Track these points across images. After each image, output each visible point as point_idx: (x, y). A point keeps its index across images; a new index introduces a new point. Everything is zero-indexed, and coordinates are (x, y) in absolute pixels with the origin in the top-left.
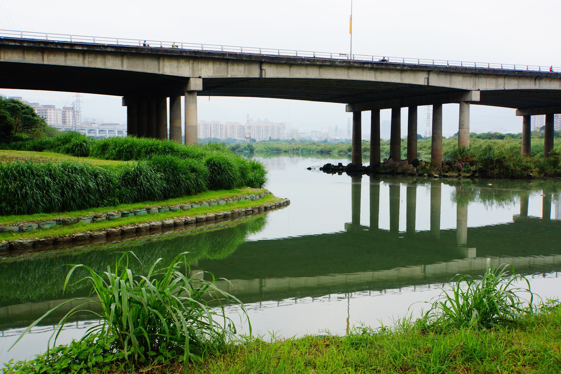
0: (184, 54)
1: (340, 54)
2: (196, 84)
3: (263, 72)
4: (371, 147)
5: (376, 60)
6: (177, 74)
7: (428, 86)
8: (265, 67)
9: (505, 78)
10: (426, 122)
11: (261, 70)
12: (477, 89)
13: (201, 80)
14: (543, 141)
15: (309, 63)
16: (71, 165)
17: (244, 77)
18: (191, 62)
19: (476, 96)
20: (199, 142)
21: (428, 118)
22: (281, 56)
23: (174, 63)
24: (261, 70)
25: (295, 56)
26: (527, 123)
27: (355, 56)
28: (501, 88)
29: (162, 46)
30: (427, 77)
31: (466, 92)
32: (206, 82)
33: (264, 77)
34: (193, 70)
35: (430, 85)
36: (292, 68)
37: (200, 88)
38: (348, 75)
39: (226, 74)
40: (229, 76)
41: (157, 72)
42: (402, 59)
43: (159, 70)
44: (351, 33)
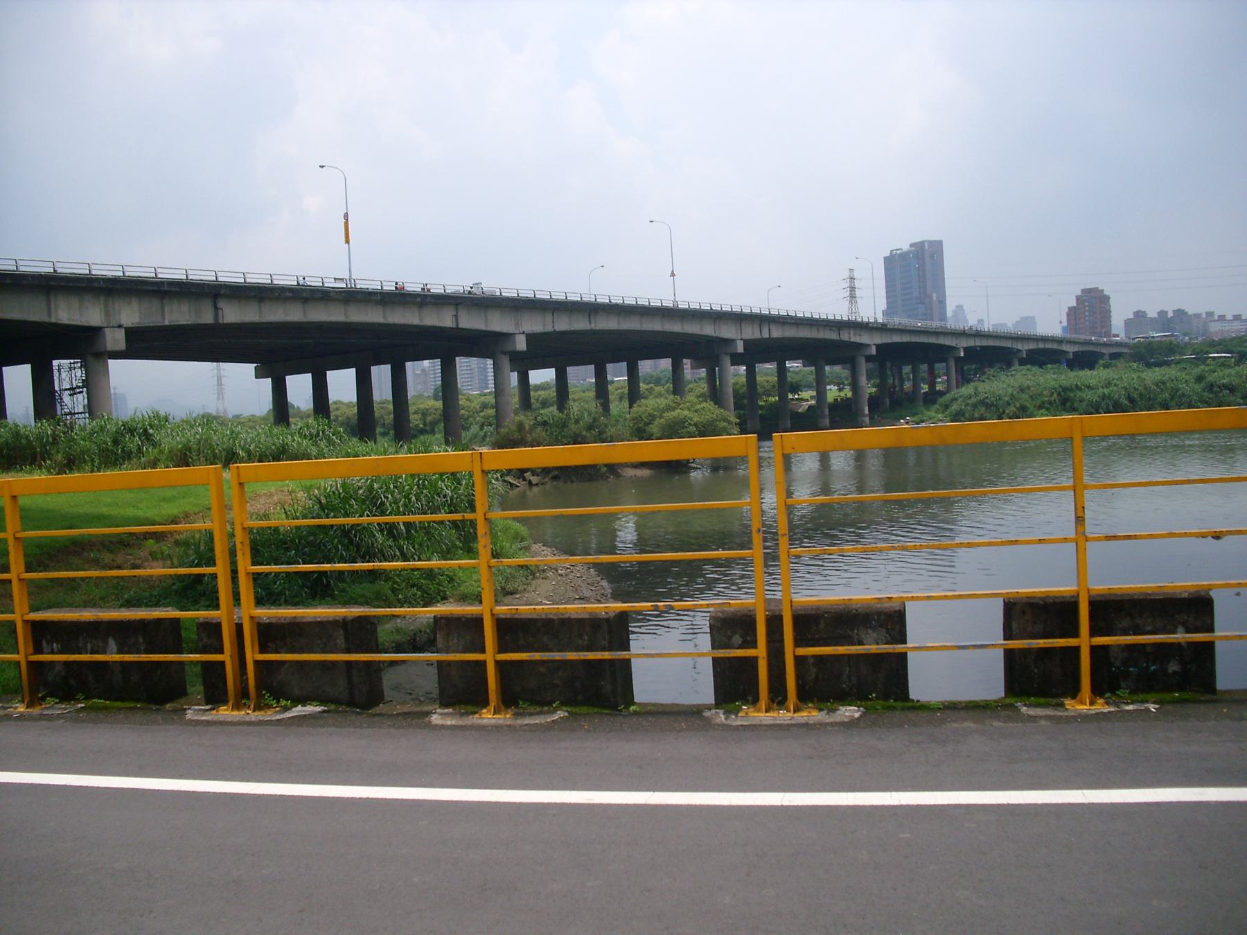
0: (96, 285)
1: (335, 279)
2: (115, 339)
3: (220, 311)
4: (557, 394)
5: (390, 287)
6: (81, 322)
7: (457, 328)
8: (222, 304)
9: (714, 322)
10: (216, 391)
11: (216, 308)
12: (521, 331)
13: (123, 331)
14: (439, 404)
15: (291, 294)
16: (419, 422)
17: (190, 323)
18: (102, 298)
19: (115, 339)
20: (305, 413)
21: (218, 385)
22: (192, 280)
23: (75, 302)
24: (216, 308)
25: (153, 278)
26: (280, 391)
27: (357, 282)
28: (549, 328)
29: (57, 269)
30: (455, 314)
31: (93, 333)
32: (131, 334)
33: (221, 322)
34: (107, 314)
35: (460, 326)
36: (262, 304)
37: (121, 345)
38: (345, 314)
39: (713, 332)
40: (167, 323)
41: (46, 319)
42: (185, 272)
43: (49, 315)
44: (347, 241)
